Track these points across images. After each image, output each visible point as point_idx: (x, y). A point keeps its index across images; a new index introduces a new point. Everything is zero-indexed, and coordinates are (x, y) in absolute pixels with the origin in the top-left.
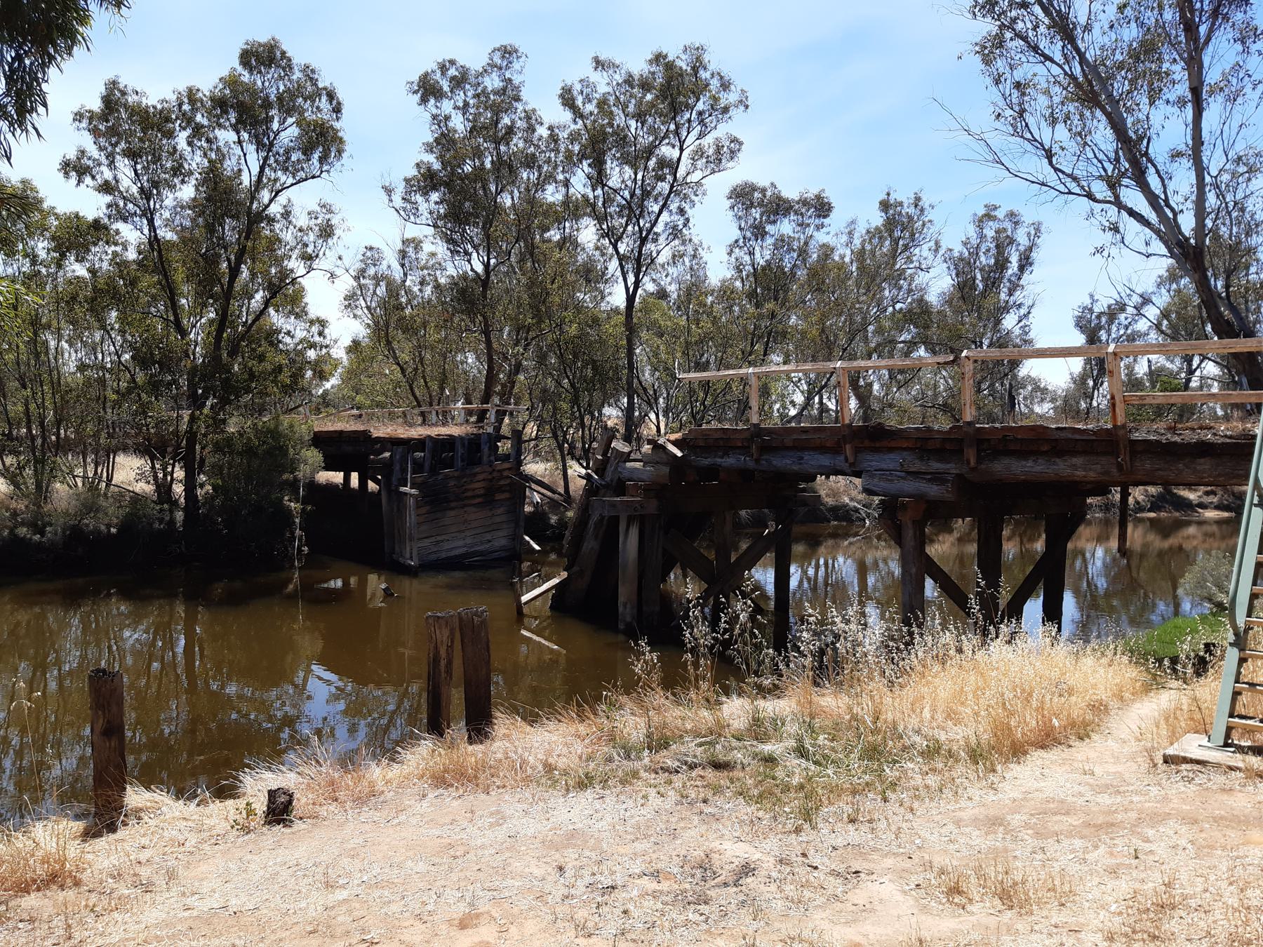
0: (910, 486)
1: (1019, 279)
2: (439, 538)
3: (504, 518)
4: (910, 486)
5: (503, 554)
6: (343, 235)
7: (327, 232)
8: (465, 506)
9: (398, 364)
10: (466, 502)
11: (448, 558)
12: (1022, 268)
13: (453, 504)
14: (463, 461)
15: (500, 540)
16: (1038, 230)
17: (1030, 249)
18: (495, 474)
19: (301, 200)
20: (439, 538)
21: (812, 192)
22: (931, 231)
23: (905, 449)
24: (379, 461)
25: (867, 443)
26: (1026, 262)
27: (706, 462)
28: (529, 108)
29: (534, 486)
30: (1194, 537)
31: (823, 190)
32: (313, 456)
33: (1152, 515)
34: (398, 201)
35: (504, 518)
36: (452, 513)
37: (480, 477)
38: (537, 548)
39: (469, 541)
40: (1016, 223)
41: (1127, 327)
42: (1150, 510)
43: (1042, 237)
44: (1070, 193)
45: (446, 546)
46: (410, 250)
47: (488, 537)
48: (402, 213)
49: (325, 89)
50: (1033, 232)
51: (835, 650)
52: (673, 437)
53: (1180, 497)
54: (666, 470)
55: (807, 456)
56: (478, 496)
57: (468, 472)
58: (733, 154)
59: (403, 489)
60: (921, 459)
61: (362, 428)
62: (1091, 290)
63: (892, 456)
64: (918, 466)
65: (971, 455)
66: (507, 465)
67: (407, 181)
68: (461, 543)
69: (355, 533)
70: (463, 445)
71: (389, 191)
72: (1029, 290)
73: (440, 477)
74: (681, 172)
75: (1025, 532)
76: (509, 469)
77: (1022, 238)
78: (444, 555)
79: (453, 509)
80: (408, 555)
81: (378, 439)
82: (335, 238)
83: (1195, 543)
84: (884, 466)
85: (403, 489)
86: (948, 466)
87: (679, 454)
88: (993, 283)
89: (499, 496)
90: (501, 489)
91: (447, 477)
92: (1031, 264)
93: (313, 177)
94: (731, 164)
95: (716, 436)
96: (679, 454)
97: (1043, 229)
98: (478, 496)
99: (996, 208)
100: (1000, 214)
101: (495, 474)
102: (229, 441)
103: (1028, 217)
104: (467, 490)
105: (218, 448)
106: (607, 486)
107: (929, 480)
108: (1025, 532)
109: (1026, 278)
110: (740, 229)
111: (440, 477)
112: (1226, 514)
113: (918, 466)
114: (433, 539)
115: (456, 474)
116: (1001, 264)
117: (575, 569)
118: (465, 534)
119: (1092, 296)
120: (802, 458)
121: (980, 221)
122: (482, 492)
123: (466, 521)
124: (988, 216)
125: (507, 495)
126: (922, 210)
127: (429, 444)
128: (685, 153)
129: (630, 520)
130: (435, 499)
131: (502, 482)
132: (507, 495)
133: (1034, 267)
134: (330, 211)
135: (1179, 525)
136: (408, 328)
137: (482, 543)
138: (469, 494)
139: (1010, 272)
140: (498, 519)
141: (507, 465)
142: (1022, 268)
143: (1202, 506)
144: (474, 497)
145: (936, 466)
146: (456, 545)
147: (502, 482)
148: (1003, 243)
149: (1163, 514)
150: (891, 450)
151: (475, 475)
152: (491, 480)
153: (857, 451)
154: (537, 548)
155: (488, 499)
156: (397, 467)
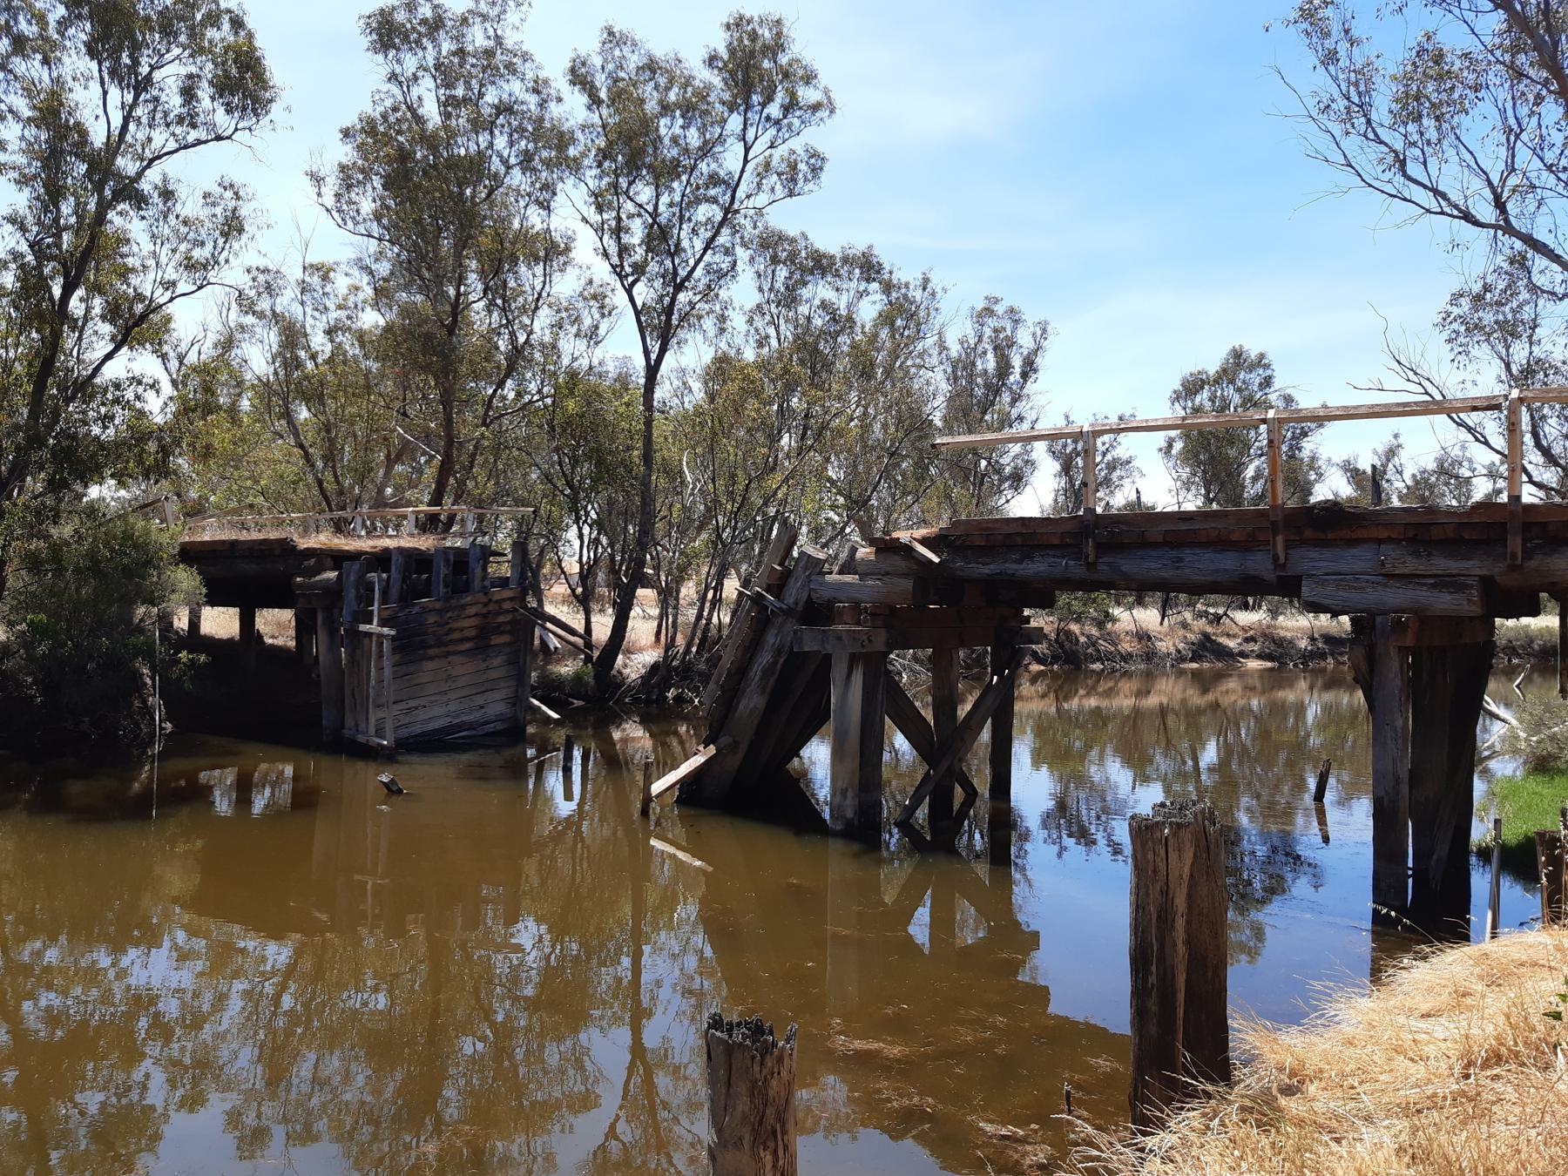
0: (1396, 596)
1: (1022, 388)
2: (412, 703)
3: (502, 672)
4: (1396, 596)
5: (500, 726)
6: (258, 235)
7: (232, 227)
8: (448, 654)
9: (301, 446)
10: (451, 648)
11: (423, 734)
12: (1025, 376)
13: (432, 652)
14: (446, 586)
15: (495, 705)
16: (1044, 331)
17: (1035, 352)
18: (492, 607)
19: (193, 174)
20: (412, 703)
21: (859, 248)
22: (937, 322)
23: (1390, 540)
24: (316, 586)
25: (1308, 533)
26: (1029, 368)
27: (985, 570)
28: (542, 75)
29: (549, 625)
30: (1234, 691)
31: (870, 247)
32: (186, 579)
33: (1195, 665)
34: (329, 200)
35: (502, 672)
36: (429, 665)
37: (472, 610)
38: (555, 716)
39: (453, 707)
40: (1016, 322)
41: (1104, 454)
42: (1192, 660)
43: (1050, 338)
44: (1442, 213)
45: (421, 715)
46: (315, 280)
47: (480, 700)
48: (336, 216)
49: (229, 11)
50: (1039, 333)
51: (579, 832)
52: (921, 532)
53: (1220, 644)
54: (908, 584)
55: (1188, 555)
56: (468, 639)
57: (454, 602)
58: (816, 171)
59: (364, 628)
60: (1416, 554)
61: (283, 536)
62: (1065, 410)
63: (1355, 551)
64: (1411, 565)
65: (1515, 543)
66: (508, 594)
67: (343, 168)
68: (438, 711)
69: (250, 703)
70: (447, 561)
71: (317, 179)
72: (1037, 400)
73: (416, 610)
74: (740, 194)
75: (1061, 687)
76: (511, 599)
77: (1025, 339)
78: (418, 729)
79: (431, 658)
80: (372, 730)
81: (310, 553)
82: (244, 237)
83: (1233, 698)
84: (1343, 567)
85: (364, 628)
86: (1469, 564)
87: (936, 560)
88: (994, 390)
89: (498, 640)
90: (498, 630)
91: (426, 610)
92: (1036, 371)
93: (219, 138)
94: (810, 186)
95: (1007, 530)
96: (936, 560)
97: (1049, 329)
98: (468, 639)
99: (997, 301)
100: (1000, 309)
101: (492, 607)
102: (56, 549)
103: (1031, 317)
104: (451, 630)
105: (33, 563)
106: (788, 612)
107: (1434, 586)
108: (1061, 687)
109: (1030, 387)
110: (761, 290)
111: (416, 610)
112: (1269, 664)
113: (1411, 565)
114: (403, 705)
115: (438, 605)
116: (1004, 368)
117: (725, 740)
118: (454, 693)
119: (1067, 417)
120: (1180, 560)
121: (979, 315)
122: (473, 633)
123: (449, 678)
124: (989, 312)
125: (506, 638)
126: (933, 294)
127: (396, 561)
128: (750, 166)
129: (853, 661)
130: (412, 645)
131: (501, 619)
132: (506, 638)
133: (1040, 375)
134: (237, 196)
135: (1219, 676)
136: (314, 394)
137: (471, 710)
138: (455, 636)
139: (1012, 378)
140: (494, 674)
141: (508, 594)
142: (1025, 376)
143: (1243, 654)
144: (461, 640)
145: (1444, 564)
146: (435, 714)
147: (501, 619)
148: (1002, 350)
149: (1206, 665)
150: (1352, 543)
151: (463, 607)
152: (485, 616)
153: (1288, 545)
154: (555, 716)
155: (481, 645)
156: (351, 594)
